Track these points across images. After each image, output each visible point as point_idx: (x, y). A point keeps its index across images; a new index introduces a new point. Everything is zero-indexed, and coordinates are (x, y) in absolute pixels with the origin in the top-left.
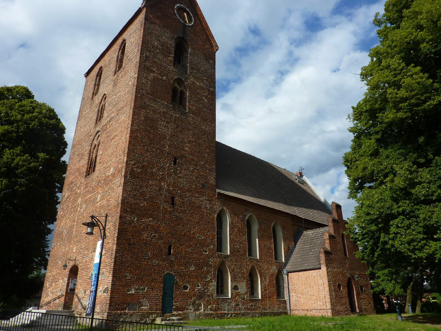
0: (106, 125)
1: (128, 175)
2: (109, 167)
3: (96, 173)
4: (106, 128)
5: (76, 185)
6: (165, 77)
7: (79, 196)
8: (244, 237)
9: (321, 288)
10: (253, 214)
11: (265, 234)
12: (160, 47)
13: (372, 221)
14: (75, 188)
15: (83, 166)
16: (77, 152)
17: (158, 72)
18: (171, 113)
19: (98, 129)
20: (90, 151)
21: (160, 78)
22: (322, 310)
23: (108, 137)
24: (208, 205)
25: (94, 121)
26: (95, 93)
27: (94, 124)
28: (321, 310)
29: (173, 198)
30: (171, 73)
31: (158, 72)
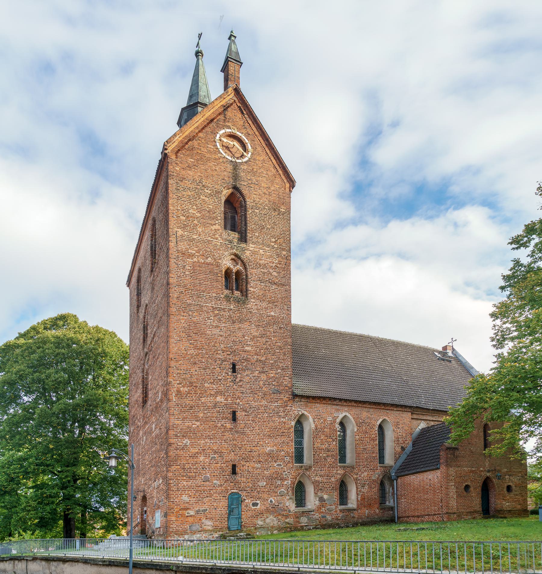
0: (151, 343)
1: (174, 397)
2: (158, 392)
3: (149, 403)
4: (152, 346)
5: (137, 418)
6: (209, 259)
7: (141, 428)
8: (334, 443)
9: (437, 491)
10: (347, 414)
11: (365, 436)
12: (198, 215)
13: (28, 455)
14: (137, 421)
15: (139, 397)
16: (134, 382)
17: (199, 254)
18: (222, 307)
19: (146, 350)
20: (143, 378)
21: (203, 261)
22: (436, 515)
23: (154, 357)
24: (282, 413)
25: (142, 341)
26: (138, 307)
27: (142, 344)
28: (435, 515)
29: (234, 413)
30: (219, 250)
31: (199, 254)
